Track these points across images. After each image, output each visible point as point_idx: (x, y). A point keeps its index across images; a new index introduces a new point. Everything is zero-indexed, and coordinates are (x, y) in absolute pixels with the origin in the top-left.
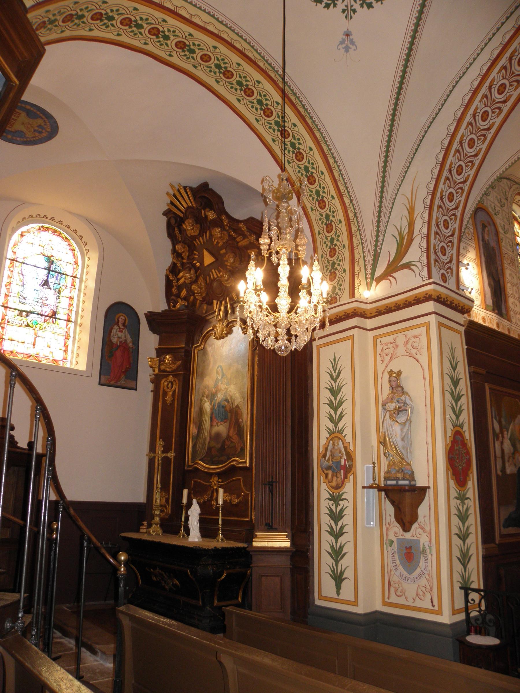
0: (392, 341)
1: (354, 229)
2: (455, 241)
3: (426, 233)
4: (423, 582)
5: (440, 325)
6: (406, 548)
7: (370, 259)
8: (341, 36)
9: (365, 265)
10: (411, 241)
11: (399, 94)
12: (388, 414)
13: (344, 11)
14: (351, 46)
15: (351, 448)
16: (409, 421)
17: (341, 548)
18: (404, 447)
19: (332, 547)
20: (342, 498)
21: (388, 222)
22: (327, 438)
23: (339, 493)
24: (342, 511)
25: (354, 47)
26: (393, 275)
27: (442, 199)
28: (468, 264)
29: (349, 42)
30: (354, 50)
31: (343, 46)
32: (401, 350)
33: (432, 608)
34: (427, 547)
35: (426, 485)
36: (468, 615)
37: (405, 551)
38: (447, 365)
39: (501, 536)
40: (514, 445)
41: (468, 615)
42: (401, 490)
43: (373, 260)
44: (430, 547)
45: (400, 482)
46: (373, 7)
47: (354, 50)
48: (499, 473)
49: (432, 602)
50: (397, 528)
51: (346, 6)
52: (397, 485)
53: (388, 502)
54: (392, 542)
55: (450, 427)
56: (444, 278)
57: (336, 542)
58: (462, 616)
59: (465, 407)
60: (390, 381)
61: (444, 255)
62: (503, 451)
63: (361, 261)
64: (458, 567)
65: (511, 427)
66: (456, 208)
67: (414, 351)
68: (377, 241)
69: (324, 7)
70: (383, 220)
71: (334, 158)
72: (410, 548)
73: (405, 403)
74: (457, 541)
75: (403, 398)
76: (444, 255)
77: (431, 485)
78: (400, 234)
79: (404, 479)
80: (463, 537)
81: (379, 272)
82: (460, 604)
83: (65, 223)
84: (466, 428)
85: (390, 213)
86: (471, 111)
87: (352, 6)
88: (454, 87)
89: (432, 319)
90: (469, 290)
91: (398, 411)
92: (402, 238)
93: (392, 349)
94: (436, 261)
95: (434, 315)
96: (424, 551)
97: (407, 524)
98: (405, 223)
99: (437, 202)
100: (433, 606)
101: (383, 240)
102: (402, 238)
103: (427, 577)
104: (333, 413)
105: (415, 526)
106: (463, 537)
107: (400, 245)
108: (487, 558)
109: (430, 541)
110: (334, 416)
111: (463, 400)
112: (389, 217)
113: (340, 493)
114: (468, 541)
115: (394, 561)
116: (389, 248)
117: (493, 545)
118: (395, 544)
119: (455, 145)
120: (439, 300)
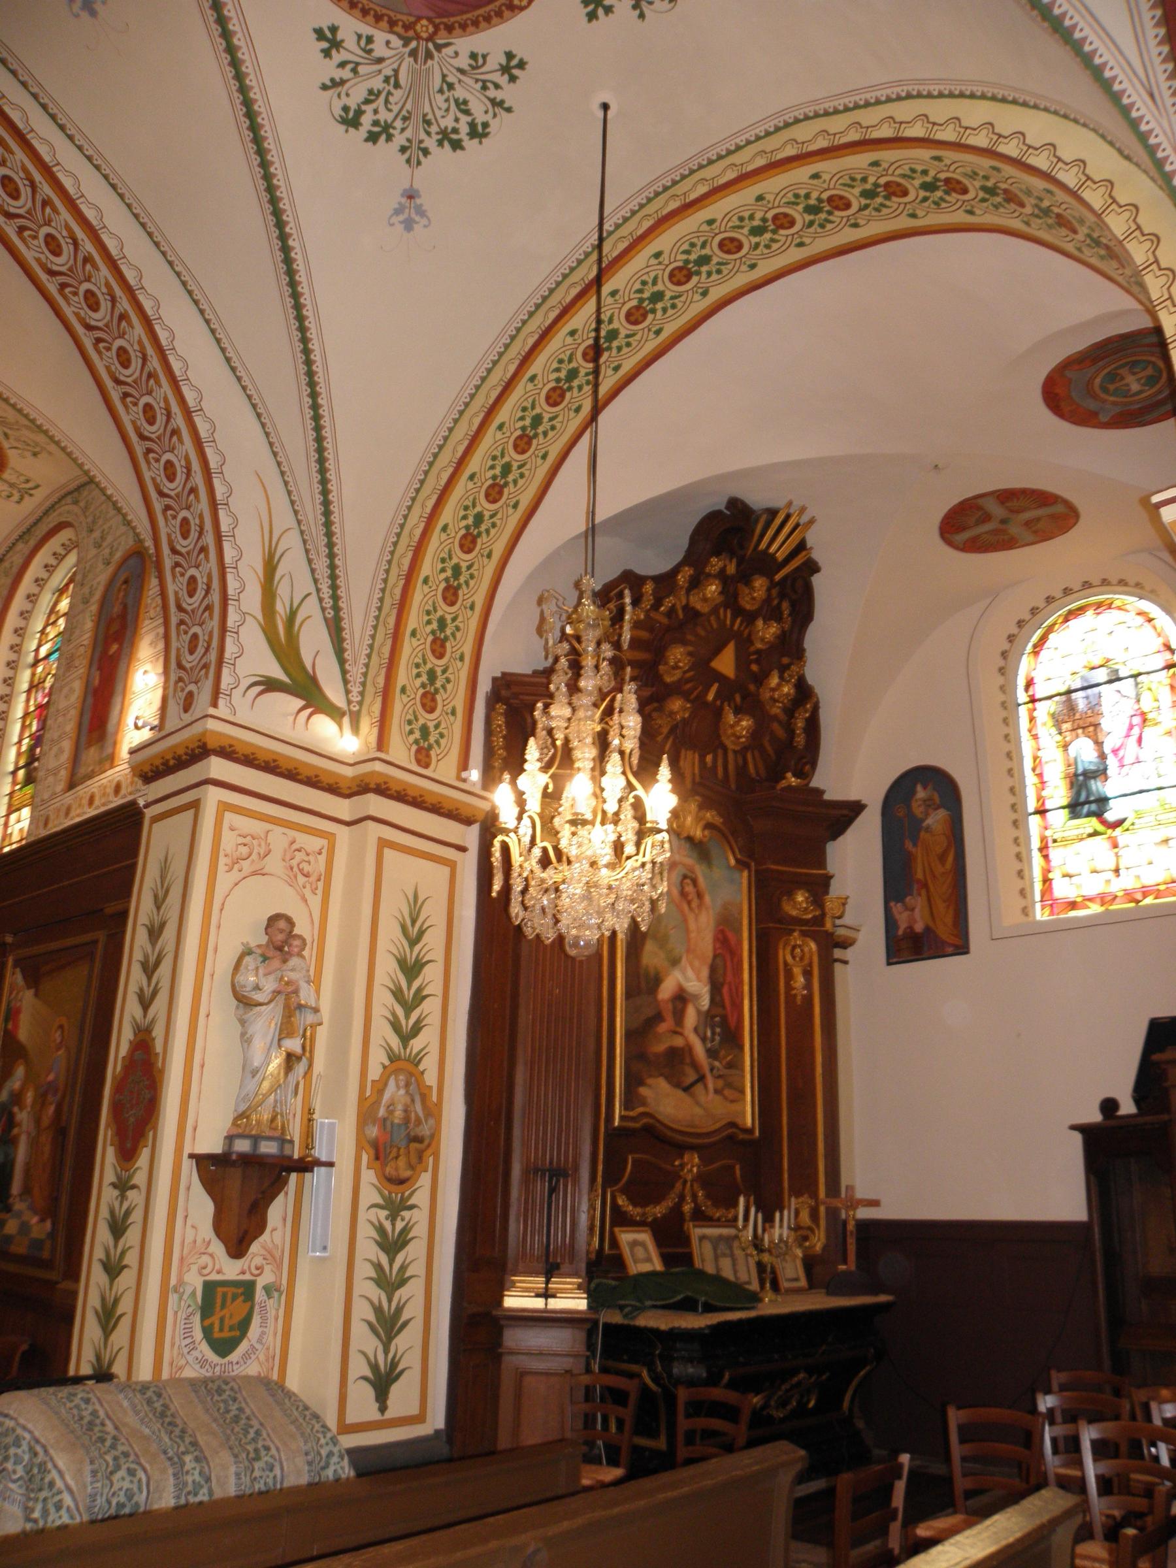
8: (395, 199)
13: (403, 150)
14: (417, 218)
17: (399, 1310)
19: (378, 1310)
20: (410, 1202)
22: (385, 1067)
23: (403, 1194)
24: (405, 1230)
25: (424, 221)
29: (413, 210)
30: (425, 226)
31: (401, 218)
39: (622, 1118)
46: (462, 148)
47: (425, 226)
51: (409, 140)
57: (390, 1301)
69: (367, 140)
83: (1058, 594)
87: (421, 142)
104: (400, 1012)
110: (403, 1022)
113: (407, 1194)
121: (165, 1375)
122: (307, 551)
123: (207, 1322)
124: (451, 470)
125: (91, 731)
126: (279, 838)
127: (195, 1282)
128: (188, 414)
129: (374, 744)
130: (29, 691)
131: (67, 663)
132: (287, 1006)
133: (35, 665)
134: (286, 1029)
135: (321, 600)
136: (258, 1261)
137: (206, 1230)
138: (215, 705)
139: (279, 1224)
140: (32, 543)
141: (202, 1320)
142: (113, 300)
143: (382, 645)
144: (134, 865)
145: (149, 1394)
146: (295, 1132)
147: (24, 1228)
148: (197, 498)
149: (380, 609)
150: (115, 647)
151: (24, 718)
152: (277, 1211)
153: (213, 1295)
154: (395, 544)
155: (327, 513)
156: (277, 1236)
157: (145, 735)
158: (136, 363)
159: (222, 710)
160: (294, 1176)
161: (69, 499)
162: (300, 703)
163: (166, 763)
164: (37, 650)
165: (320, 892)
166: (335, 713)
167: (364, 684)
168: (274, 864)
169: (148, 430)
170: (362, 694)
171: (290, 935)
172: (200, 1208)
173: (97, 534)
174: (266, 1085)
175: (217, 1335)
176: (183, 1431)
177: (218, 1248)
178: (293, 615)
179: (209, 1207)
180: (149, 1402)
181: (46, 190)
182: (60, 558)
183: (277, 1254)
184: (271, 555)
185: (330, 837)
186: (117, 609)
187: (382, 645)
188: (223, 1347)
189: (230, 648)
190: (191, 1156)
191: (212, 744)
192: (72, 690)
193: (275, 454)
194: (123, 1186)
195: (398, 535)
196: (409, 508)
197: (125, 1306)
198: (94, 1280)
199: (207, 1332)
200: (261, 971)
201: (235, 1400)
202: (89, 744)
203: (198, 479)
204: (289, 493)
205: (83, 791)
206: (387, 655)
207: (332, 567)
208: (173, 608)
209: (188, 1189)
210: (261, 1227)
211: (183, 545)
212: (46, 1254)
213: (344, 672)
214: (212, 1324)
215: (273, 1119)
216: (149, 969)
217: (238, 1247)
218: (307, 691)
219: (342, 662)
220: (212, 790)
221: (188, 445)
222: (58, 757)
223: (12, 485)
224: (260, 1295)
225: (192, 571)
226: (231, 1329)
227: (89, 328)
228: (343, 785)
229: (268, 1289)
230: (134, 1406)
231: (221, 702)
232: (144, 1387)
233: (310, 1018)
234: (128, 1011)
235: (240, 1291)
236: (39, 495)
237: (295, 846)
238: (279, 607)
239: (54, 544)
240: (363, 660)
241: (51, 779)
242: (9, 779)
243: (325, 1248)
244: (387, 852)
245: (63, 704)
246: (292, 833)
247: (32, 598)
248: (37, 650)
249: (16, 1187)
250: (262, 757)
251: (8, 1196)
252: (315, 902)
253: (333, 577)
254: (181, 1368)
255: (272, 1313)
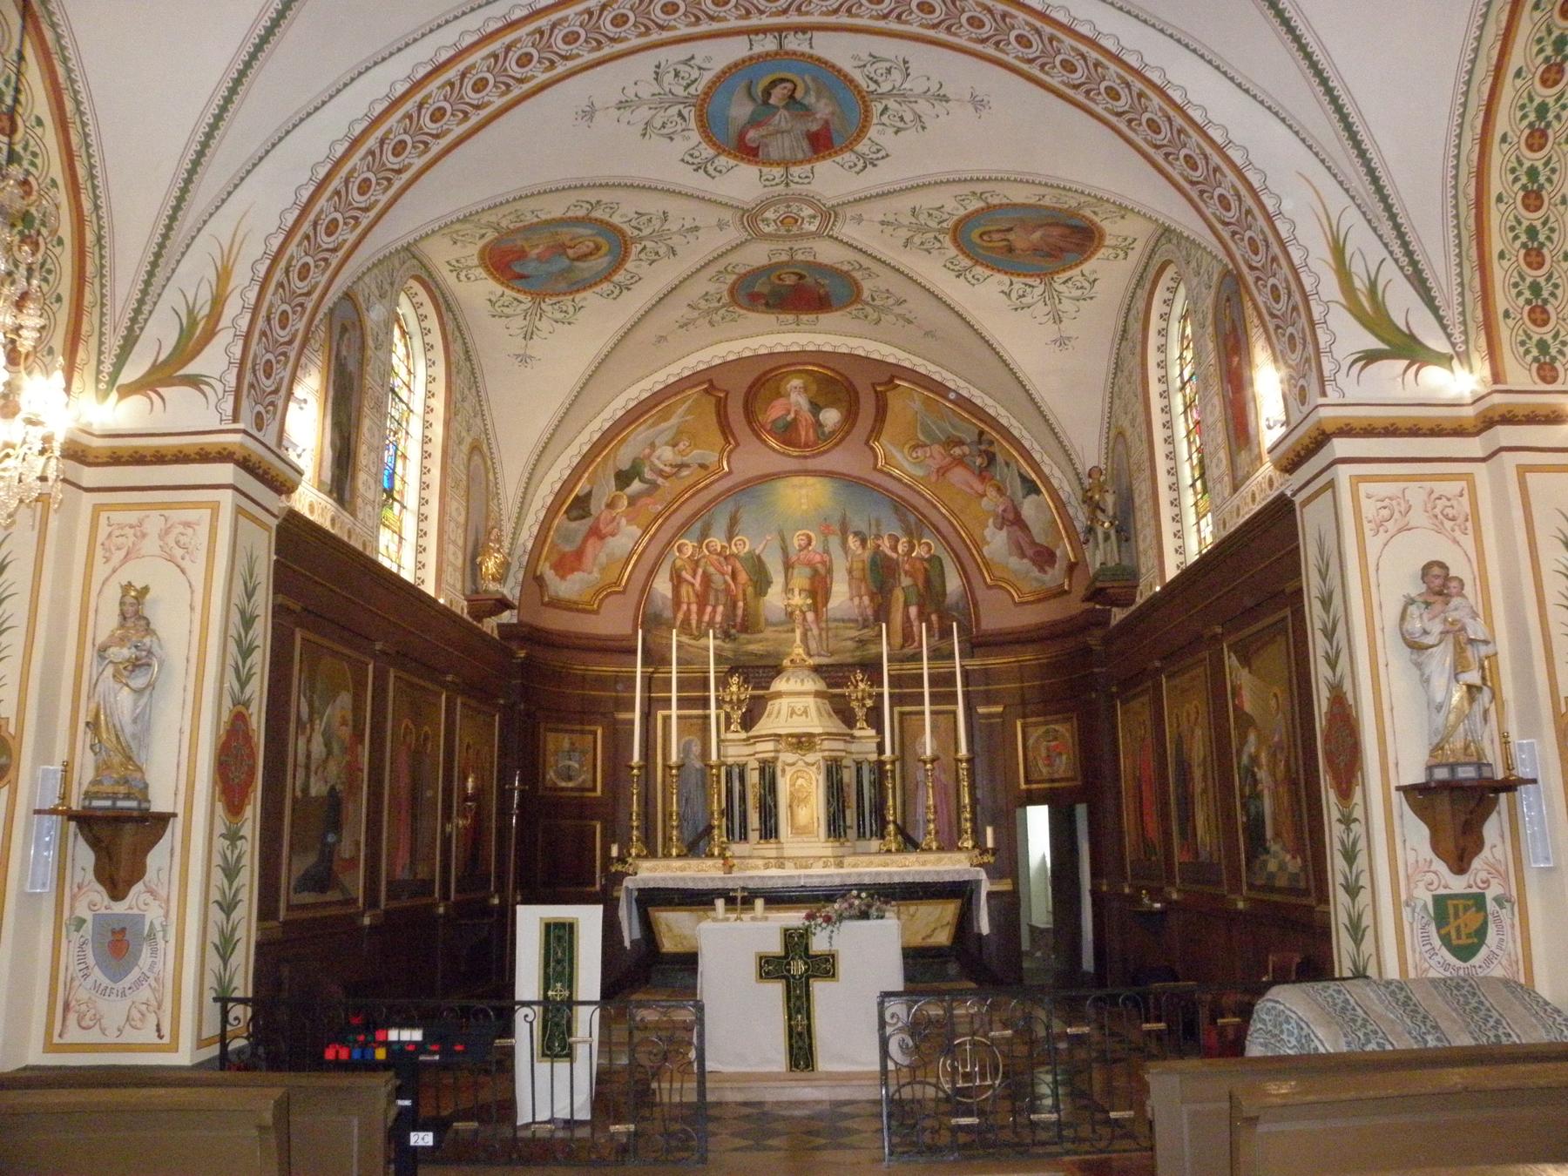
0: (134, 521)
1: (90, 269)
2: (293, 355)
3: (245, 328)
4: (145, 993)
5: (239, 511)
6: (114, 932)
7: (113, 343)
9: (100, 353)
10: (210, 334)
11: (259, 48)
12: (110, 670)
15: (12, 729)
16: (151, 685)
18: (134, 736)
21: (168, 279)
26: (160, 390)
27: (287, 272)
28: (305, 401)
32: (151, 545)
33: (158, 1041)
34: (158, 928)
35: (170, 810)
36: (224, 1046)
37: (109, 937)
38: (239, 588)
39: (290, 908)
40: (327, 744)
41: (224, 1046)
42: (117, 819)
43: (121, 347)
44: (164, 928)
45: (120, 804)
48: (299, 794)
49: (158, 1030)
50: (98, 894)
52: (114, 808)
53: (81, 843)
54: (81, 922)
55: (227, 703)
56: (259, 422)
58: (215, 1050)
59: (257, 669)
60: (122, 603)
61: (268, 377)
62: (308, 756)
63: (94, 341)
64: (214, 961)
65: (328, 712)
66: (308, 294)
67: (178, 552)
68: (138, 311)
70: (160, 274)
71: (78, 103)
72: (123, 930)
73: (150, 652)
74: (217, 915)
75: (147, 640)
76: (268, 377)
77: (180, 811)
78: (190, 312)
79: (128, 797)
80: (228, 907)
81: (130, 374)
82: (212, 1028)
84: (254, 708)
85: (178, 262)
86: (379, 133)
88: (360, 74)
89: (227, 498)
90: (299, 451)
91: (137, 665)
92: (193, 322)
93: (132, 539)
94: (252, 386)
95: (230, 492)
96: (151, 936)
97: (121, 886)
98: (205, 295)
99: (278, 275)
100: (161, 1037)
101: (151, 312)
102: (193, 322)
103: (154, 984)
105: (138, 888)
106: (228, 907)
107: (185, 333)
108: (262, 948)
109: (166, 915)
111: (257, 657)
112: (173, 271)
114: (235, 915)
115: (82, 959)
116: (160, 334)
117: (275, 923)
118: (89, 926)
119: (336, 183)
120: (247, 464)
121: (1412, 975)
122: (1369, 221)
123: (1443, 932)
124: (1490, 80)
125: (1237, 438)
126: (1416, 493)
127: (1425, 897)
128: (1220, 150)
129: (1489, 378)
130: (1185, 412)
131: (1204, 385)
132: (1457, 643)
133: (1183, 388)
134: (1459, 667)
135: (1396, 261)
136: (1483, 875)
137: (1426, 851)
138: (1324, 394)
139: (1498, 841)
140: (1148, 286)
141: (1438, 929)
142: (1128, 85)
143: (1472, 279)
144: (1298, 547)
145: (1392, 987)
146: (1493, 755)
147: (1282, 866)
148: (1254, 218)
149: (1459, 245)
150: (1236, 359)
151: (1188, 436)
152: (1492, 829)
153: (1443, 908)
154: (1456, 177)
155: (1375, 180)
156: (1498, 853)
157: (1279, 431)
158: (1165, 127)
159: (1333, 396)
160: (1503, 796)
161: (1163, 240)
162: (1406, 362)
163: (1298, 455)
164: (1181, 375)
165: (1470, 531)
166: (1443, 360)
167: (1464, 323)
168: (1418, 517)
169: (1195, 176)
170: (1465, 333)
171: (1447, 578)
172: (1417, 834)
173: (1193, 264)
174: (1452, 717)
175: (1455, 942)
176: (1425, 1017)
177: (1440, 866)
178: (1373, 285)
179: (1425, 831)
180: (1393, 993)
181: (1048, 30)
182: (1173, 291)
183: (1502, 869)
184: (1336, 240)
185: (1469, 478)
186: (1228, 326)
187: (1472, 279)
188: (1465, 952)
189: (1323, 338)
190: (1398, 788)
191: (1329, 429)
192: (1214, 406)
193: (1310, 147)
194: (1347, 820)
195: (1457, 167)
196: (1459, 136)
197: (1367, 920)
198: (1340, 901)
199: (1446, 940)
200: (1425, 617)
201: (1474, 994)
202: (1240, 449)
203: (1249, 202)
204: (1335, 176)
205: (1245, 490)
206: (1478, 288)
207: (1397, 227)
208: (1267, 318)
209: (1401, 817)
210: (1479, 845)
211: (1257, 261)
212: (1302, 885)
213: (1440, 319)
214: (1449, 934)
215: (1467, 747)
216: (1329, 634)
217: (1460, 864)
218: (1408, 348)
219: (1435, 310)
220: (1341, 468)
221: (1231, 176)
222: (1219, 467)
223: (1114, 247)
224: (1491, 906)
225: (1272, 281)
226: (1469, 936)
227: (1119, 114)
228: (1468, 426)
229: (1499, 901)
230: (1379, 997)
231: (1329, 389)
232: (1389, 983)
233: (1484, 650)
234: (1321, 673)
235: (1470, 902)
236: (1139, 246)
237: (1434, 496)
238: (1358, 284)
239: (1165, 281)
240: (1456, 299)
241: (1218, 486)
242: (1191, 491)
243: (1547, 859)
244: (1531, 478)
245: (1210, 420)
246: (1428, 485)
247: (1163, 333)
248: (1181, 375)
249: (1269, 834)
250: (1379, 425)
251: (1265, 840)
252: (1468, 542)
253: (1401, 235)
254: (1426, 970)
255: (1507, 922)
